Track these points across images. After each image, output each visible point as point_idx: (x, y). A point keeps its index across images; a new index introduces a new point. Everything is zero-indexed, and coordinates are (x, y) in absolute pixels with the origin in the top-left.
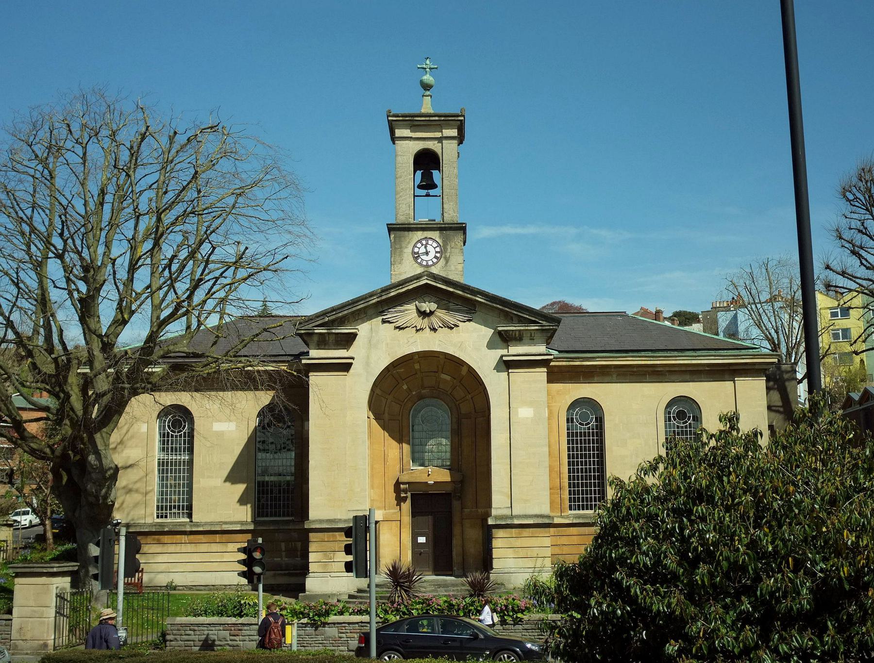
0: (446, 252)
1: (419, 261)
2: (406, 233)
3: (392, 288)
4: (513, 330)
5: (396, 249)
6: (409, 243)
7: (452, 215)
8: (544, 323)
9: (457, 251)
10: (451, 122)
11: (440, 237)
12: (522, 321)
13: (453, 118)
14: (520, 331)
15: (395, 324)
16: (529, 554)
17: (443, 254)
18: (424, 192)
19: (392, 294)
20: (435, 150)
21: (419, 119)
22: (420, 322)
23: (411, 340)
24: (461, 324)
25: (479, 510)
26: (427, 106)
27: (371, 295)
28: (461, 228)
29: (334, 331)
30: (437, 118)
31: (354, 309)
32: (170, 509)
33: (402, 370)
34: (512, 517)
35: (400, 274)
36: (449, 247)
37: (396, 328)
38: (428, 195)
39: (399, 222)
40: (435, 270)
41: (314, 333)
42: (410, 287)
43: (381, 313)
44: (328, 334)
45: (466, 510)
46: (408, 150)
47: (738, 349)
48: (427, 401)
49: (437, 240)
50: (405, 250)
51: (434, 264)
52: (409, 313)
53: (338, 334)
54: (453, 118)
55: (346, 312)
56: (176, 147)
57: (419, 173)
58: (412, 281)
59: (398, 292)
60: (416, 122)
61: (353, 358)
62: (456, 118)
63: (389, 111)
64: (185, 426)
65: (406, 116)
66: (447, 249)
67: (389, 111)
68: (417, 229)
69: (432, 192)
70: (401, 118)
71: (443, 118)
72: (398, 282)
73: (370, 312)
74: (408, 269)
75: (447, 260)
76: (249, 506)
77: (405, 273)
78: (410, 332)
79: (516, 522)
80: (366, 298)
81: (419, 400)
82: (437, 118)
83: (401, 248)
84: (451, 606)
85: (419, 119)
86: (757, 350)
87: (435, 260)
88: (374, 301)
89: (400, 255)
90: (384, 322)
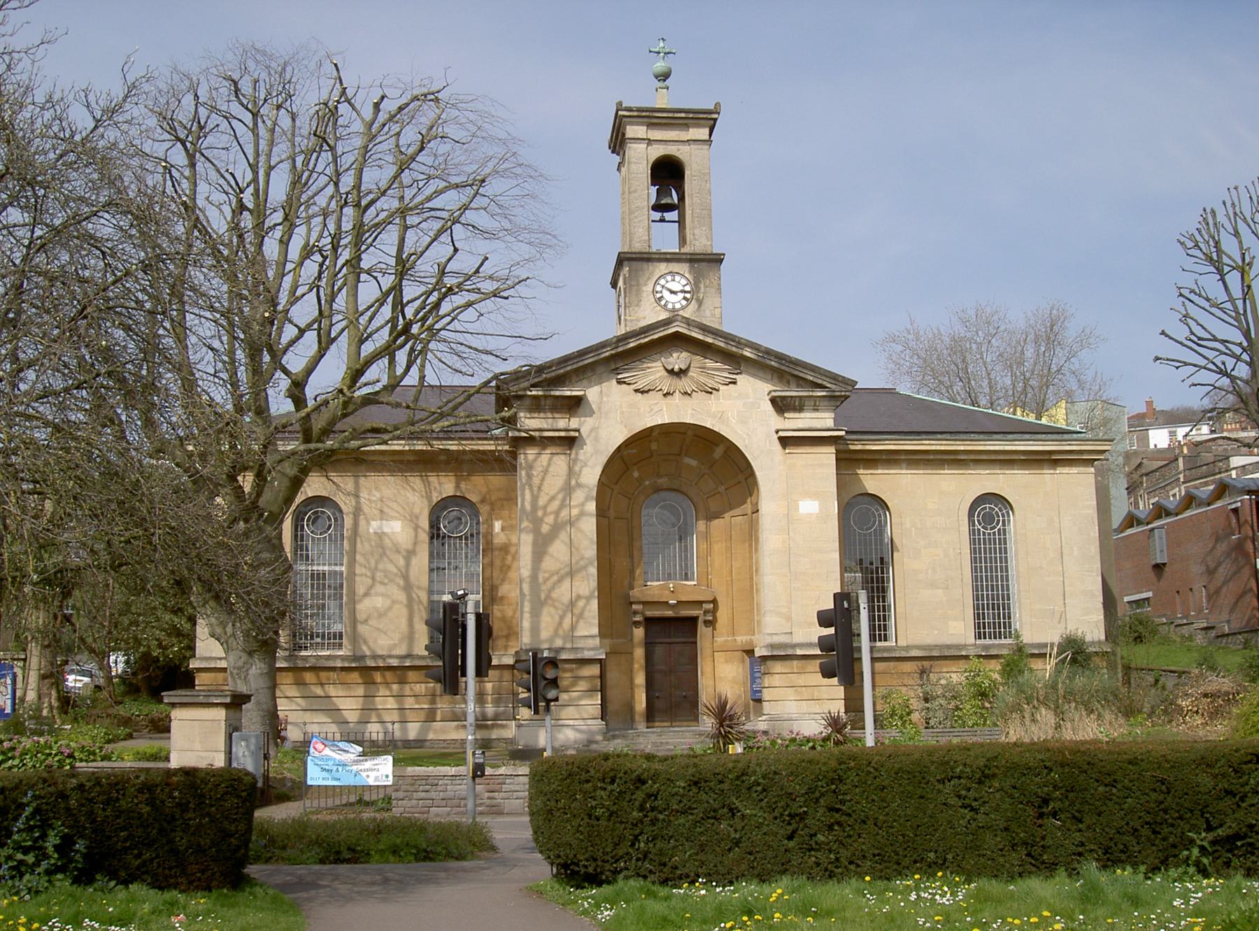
0: (698, 292)
1: (663, 303)
2: (645, 265)
3: (631, 338)
4: (792, 397)
5: (633, 287)
6: (649, 278)
7: (698, 242)
8: (833, 387)
9: (713, 290)
10: (702, 122)
11: (690, 272)
12: (802, 382)
13: (705, 116)
14: (800, 397)
15: (633, 387)
16: (816, 694)
17: (694, 295)
18: (657, 215)
19: (632, 345)
20: (680, 157)
21: (660, 115)
22: (667, 383)
23: (656, 409)
24: (722, 388)
25: (739, 639)
26: (662, 100)
27: (603, 345)
28: (717, 260)
29: (553, 393)
30: (683, 115)
31: (581, 364)
32: (312, 638)
33: (635, 451)
34: (794, 646)
35: (638, 320)
36: (702, 286)
37: (636, 391)
38: (662, 220)
39: (633, 250)
40: (687, 314)
41: (526, 396)
42: (655, 337)
43: (616, 371)
44: (545, 397)
45: (718, 639)
46: (642, 156)
47: (1058, 433)
48: (663, 494)
49: (687, 275)
50: (644, 288)
51: (683, 308)
52: (653, 371)
53: (557, 397)
54: (705, 116)
55: (569, 368)
56: (382, 117)
57: (654, 190)
58: (657, 328)
59: (638, 342)
60: (653, 118)
61: (785, 442)
62: (709, 116)
63: (620, 103)
64: (999, 521)
65: (643, 111)
66: (700, 288)
67: (620, 103)
68: (660, 260)
69: (668, 216)
70: (635, 114)
71: (691, 116)
72: (641, 328)
73: (601, 369)
74: (648, 314)
75: (700, 303)
76: (861, 471)
77: (645, 318)
78: (655, 397)
79: (799, 652)
80: (597, 350)
81: (655, 492)
82: (683, 115)
83: (638, 285)
84: (308, 917)
85: (660, 115)
86: (1083, 435)
87: (684, 303)
88: (607, 354)
89: (637, 295)
90: (620, 382)
